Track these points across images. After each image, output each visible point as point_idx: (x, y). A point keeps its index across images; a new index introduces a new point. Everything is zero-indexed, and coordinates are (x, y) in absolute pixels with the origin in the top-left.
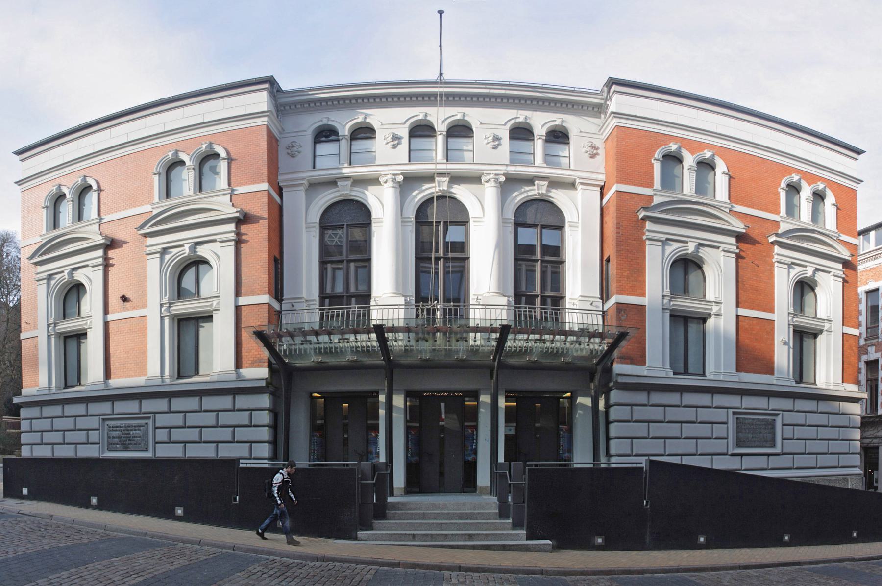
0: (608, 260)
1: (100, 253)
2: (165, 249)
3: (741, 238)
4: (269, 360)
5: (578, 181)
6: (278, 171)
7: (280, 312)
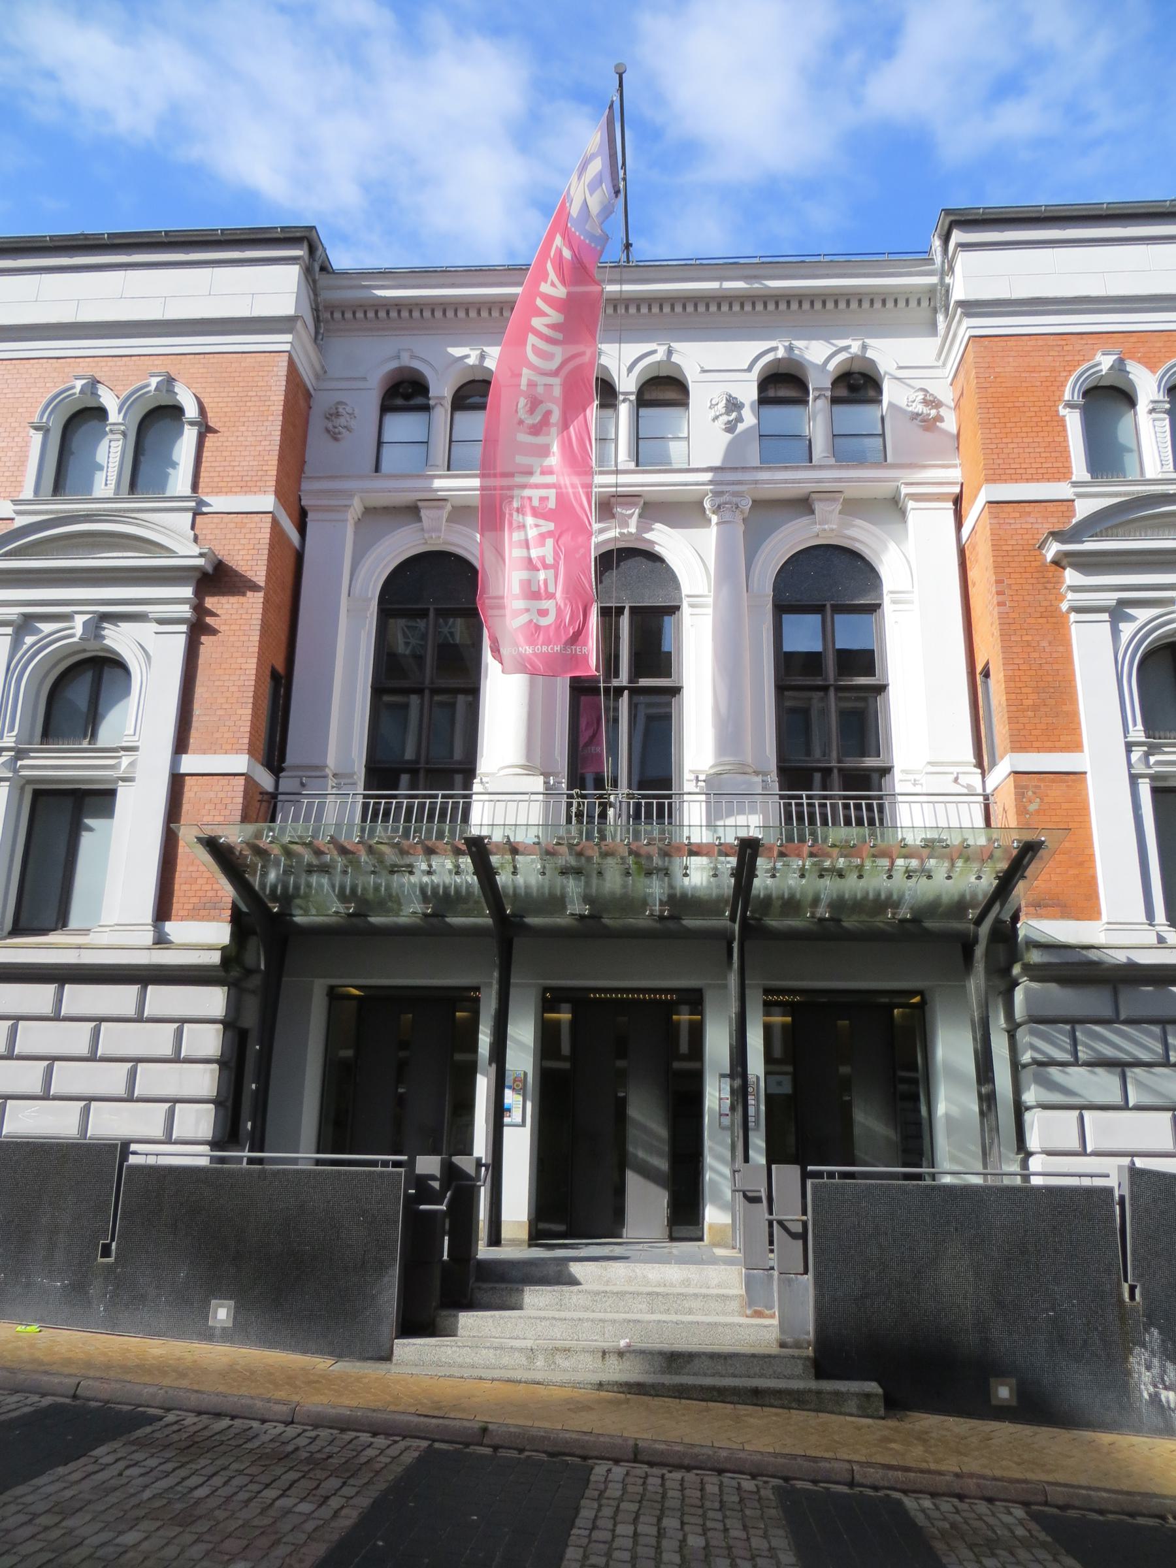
0: (986, 674)
2: (28, 619)
4: (235, 909)
6: (302, 471)
7: (274, 796)
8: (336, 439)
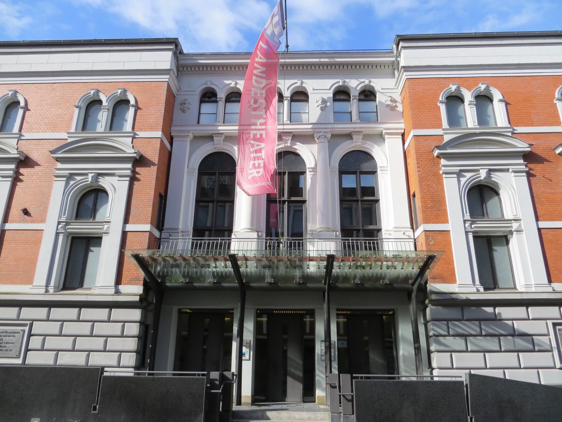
0: (414, 196)
1: (13, 166)
3: (529, 157)
5: (384, 131)
6: (172, 123)
7: (160, 239)
8: (184, 112)
